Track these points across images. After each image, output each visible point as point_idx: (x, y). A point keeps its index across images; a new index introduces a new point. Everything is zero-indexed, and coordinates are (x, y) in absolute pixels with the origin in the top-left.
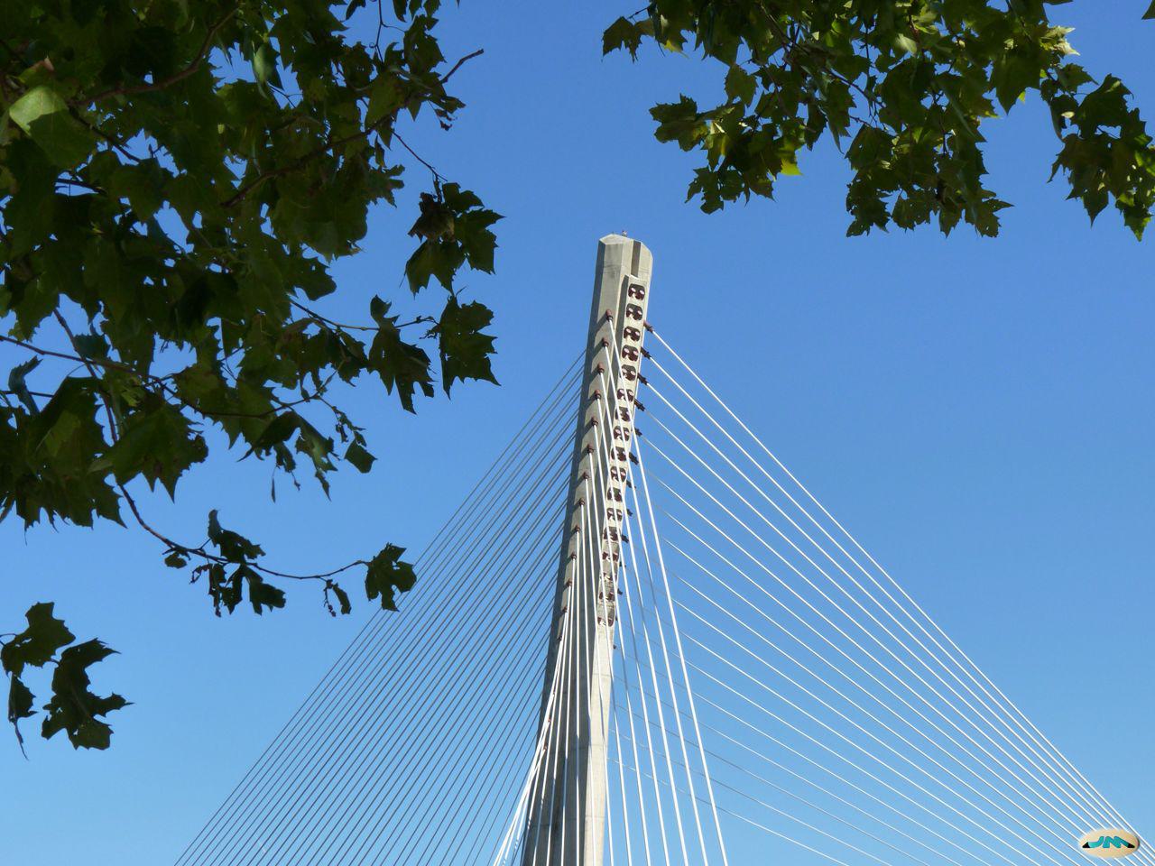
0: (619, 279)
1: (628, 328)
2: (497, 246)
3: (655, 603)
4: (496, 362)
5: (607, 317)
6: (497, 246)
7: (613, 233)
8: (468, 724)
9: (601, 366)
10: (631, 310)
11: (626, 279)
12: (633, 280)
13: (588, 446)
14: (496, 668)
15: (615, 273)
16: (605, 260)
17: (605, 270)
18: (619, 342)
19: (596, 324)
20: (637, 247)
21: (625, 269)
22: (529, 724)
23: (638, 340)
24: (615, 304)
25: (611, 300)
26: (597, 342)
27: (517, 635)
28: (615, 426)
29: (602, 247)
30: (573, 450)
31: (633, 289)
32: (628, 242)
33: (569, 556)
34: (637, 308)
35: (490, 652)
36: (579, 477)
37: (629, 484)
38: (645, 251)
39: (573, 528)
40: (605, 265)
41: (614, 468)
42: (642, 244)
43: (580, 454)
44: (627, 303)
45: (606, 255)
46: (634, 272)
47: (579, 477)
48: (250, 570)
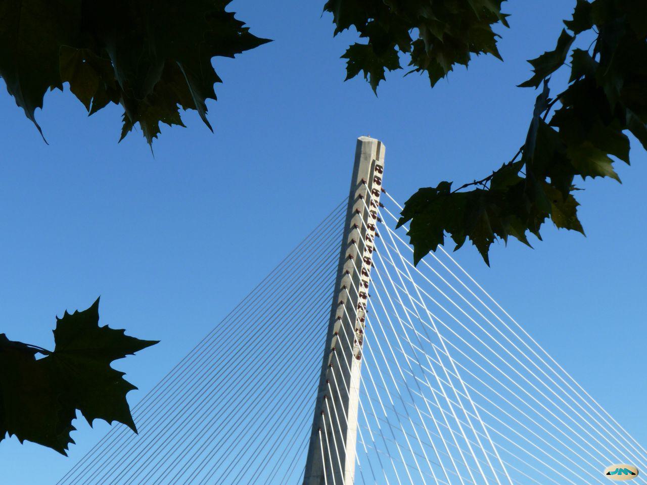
0: (369, 162)
1: (374, 189)
2: (493, 172)
3: (380, 430)
4: (470, 63)
5: (363, 182)
6: (493, 172)
7: (363, 135)
8: (155, 397)
9: (359, 210)
10: (378, 168)
11: (374, 162)
12: (377, 163)
13: (350, 255)
14: (194, 427)
15: (368, 157)
16: (362, 150)
17: (362, 156)
18: (370, 186)
19: (354, 186)
20: (379, 144)
21: (373, 156)
22: (317, 362)
23: (378, 196)
24: (367, 174)
25: (365, 172)
26: (356, 195)
27: (250, 425)
28: (363, 256)
29: (360, 143)
30: (346, 214)
31: (378, 168)
32: (375, 141)
33: (336, 317)
34: (379, 178)
35: (154, 442)
36: (343, 273)
37: (379, 220)
38: (383, 147)
39: (339, 301)
40: (362, 152)
41: (364, 269)
42: (382, 143)
43: (344, 259)
44: (375, 165)
45: (362, 147)
46: (378, 158)
47: (343, 273)
48: (457, 193)
